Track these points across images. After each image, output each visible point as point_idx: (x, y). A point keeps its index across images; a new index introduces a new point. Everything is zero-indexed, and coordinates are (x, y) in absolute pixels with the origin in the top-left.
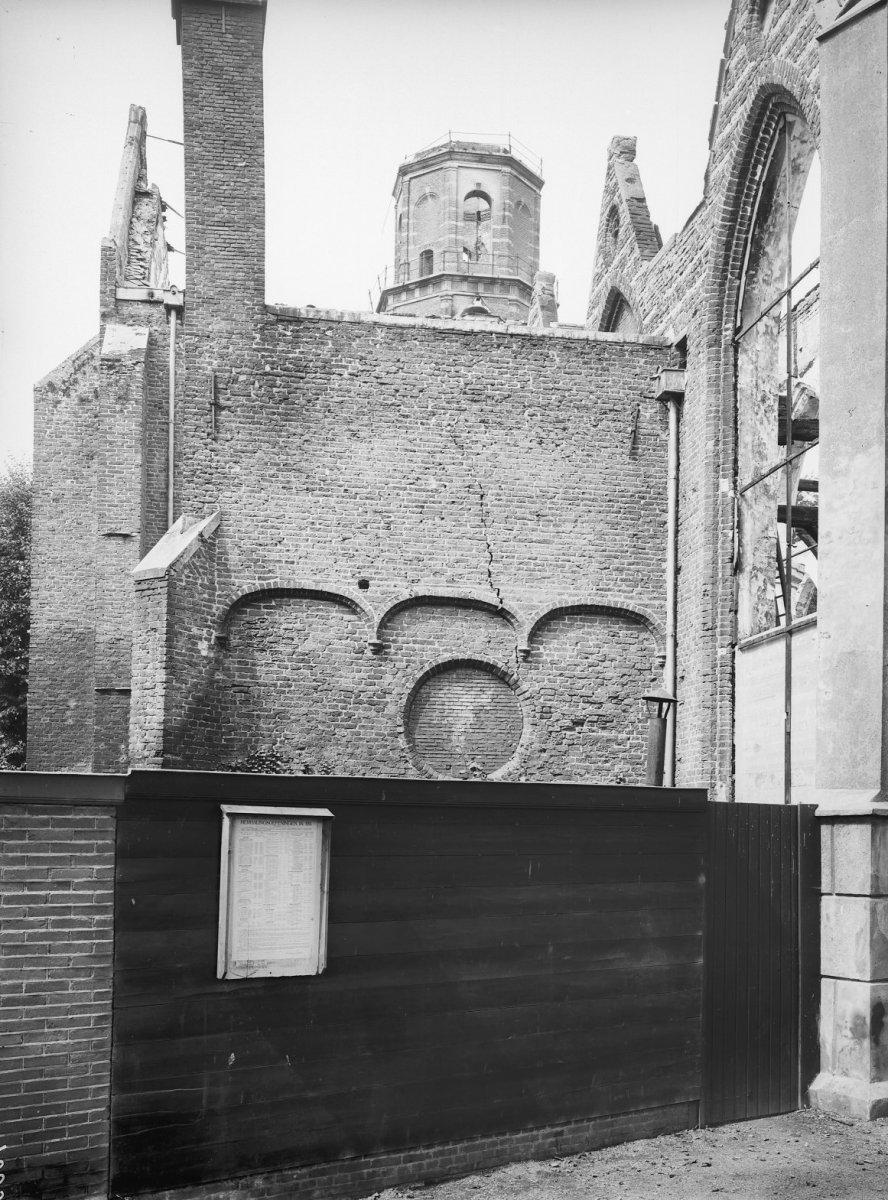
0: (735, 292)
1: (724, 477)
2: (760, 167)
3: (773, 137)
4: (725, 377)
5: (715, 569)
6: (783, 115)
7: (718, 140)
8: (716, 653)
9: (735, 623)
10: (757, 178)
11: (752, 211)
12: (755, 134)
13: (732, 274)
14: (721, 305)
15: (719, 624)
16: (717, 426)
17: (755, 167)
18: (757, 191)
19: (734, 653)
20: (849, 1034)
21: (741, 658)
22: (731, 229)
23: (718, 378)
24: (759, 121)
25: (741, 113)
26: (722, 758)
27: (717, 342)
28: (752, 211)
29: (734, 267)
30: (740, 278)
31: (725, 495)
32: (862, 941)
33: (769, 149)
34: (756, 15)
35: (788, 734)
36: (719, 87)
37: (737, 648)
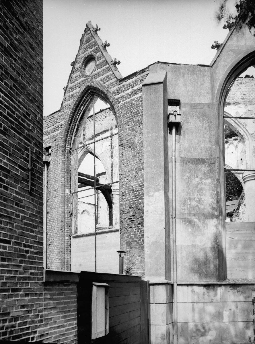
0: (71, 138)
1: (67, 188)
2: (82, 107)
3: (88, 100)
4: (67, 161)
5: (65, 214)
6: (93, 95)
7: (67, 95)
8: (65, 238)
9: (71, 230)
10: (81, 109)
11: (78, 117)
12: (83, 97)
13: (70, 133)
14: (66, 140)
15: (66, 230)
16: (65, 174)
17: (81, 106)
18: (81, 112)
19: (71, 238)
20: (160, 339)
21: (72, 240)
22: (72, 121)
23: (65, 161)
24: (85, 94)
25: (78, 91)
26: (67, 268)
27: (65, 150)
28: (78, 117)
29: (71, 131)
30: (72, 134)
31: (67, 194)
32: (163, 315)
33: (86, 103)
34: (84, 65)
35: (96, 261)
36: (69, 81)
37: (71, 237)
